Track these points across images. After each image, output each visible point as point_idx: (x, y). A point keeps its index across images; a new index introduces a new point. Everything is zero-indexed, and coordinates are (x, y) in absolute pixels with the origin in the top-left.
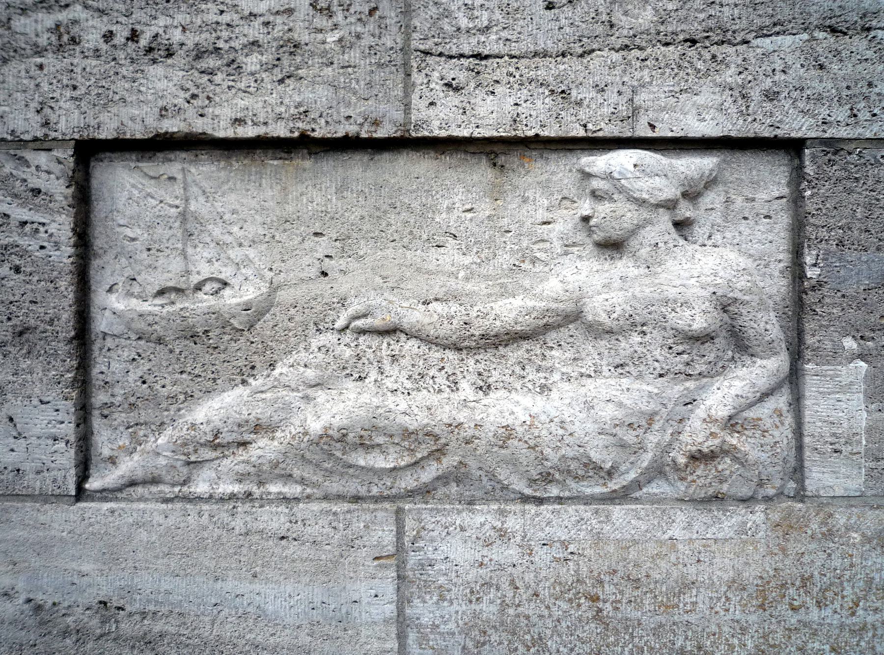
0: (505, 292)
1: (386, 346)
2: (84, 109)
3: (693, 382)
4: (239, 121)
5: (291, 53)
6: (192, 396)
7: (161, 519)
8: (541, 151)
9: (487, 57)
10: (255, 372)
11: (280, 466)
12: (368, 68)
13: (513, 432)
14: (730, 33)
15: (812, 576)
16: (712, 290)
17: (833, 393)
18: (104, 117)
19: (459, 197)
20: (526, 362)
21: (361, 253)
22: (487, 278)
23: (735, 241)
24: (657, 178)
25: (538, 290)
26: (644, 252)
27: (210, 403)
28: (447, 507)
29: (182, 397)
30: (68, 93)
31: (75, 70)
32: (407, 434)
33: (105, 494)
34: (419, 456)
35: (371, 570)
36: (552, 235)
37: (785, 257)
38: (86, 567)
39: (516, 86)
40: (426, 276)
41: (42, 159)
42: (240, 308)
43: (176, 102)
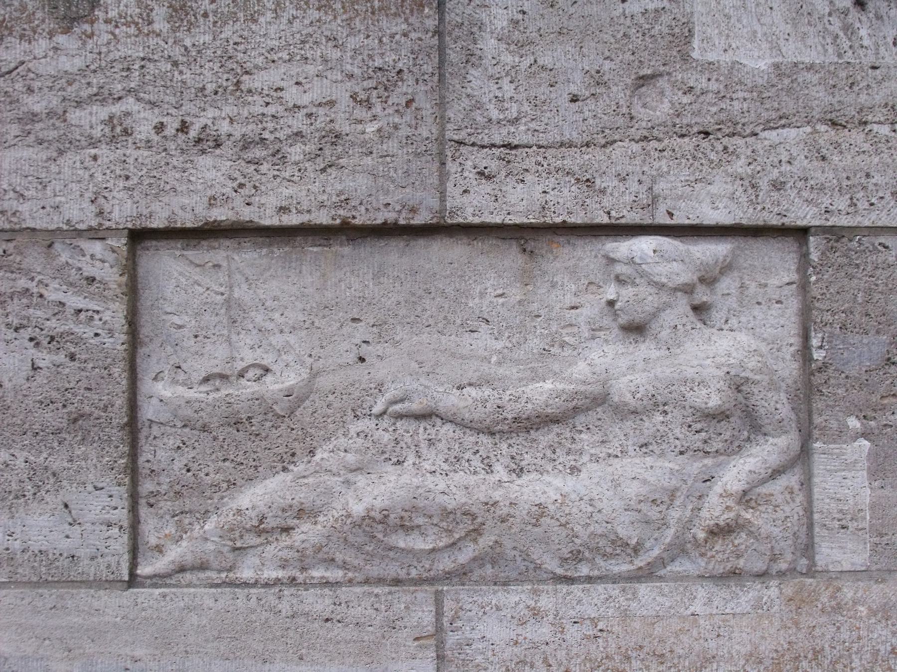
0: (536, 377)
1: (422, 430)
2: (137, 198)
3: (711, 460)
4: (283, 210)
5: (333, 143)
6: (234, 484)
7: (210, 602)
8: (568, 238)
9: (516, 147)
10: (295, 459)
11: (324, 549)
12: (406, 157)
13: (546, 510)
14: (740, 125)
15: (823, 649)
16: (726, 369)
17: (840, 470)
18: (156, 207)
19: (491, 282)
20: (556, 445)
21: (398, 338)
22: (518, 362)
23: (750, 326)
24: (675, 263)
25: (566, 374)
26: (665, 334)
27: (252, 491)
28: (484, 587)
29: (225, 485)
30: (121, 184)
31: (128, 161)
32: (446, 513)
33: (159, 579)
34: (457, 536)
35: (412, 650)
36: (580, 319)
37: (796, 341)
38: (139, 653)
39: (544, 174)
40: (461, 361)
41: (97, 248)
42: (282, 394)
43: (224, 191)
